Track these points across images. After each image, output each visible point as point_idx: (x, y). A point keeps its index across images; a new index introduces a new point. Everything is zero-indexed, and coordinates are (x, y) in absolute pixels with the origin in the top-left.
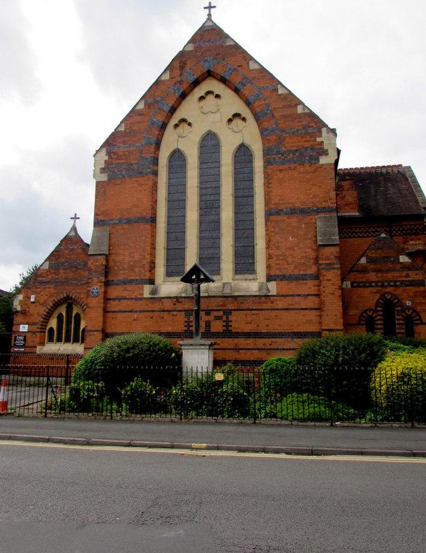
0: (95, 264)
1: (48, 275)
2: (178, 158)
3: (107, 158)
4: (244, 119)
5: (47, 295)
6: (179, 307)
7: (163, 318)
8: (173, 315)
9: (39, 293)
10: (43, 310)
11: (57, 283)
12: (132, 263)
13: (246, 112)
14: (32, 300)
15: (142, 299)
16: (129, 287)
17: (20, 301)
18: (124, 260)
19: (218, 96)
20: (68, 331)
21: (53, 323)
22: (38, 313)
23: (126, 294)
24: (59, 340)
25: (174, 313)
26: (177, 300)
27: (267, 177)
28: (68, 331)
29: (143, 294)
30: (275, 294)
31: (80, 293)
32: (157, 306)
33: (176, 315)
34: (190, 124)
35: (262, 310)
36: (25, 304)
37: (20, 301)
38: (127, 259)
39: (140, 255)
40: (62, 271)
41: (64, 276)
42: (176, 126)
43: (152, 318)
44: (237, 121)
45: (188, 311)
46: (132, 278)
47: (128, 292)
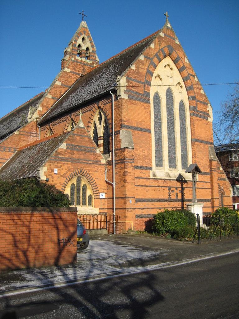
0: (129, 154)
1: (65, 154)
2: (157, 96)
5: (66, 169)
6: (166, 185)
7: (159, 190)
8: (163, 189)
9: (60, 167)
10: (63, 180)
12: (144, 156)
13: (182, 83)
14: (56, 172)
15: (150, 179)
16: (144, 171)
17: (45, 172)
18: (140, 153)
19: (171, 69)
20: (78, 197)
22: (60, 183)
23: (142, 175)
25: (164, 188)
26: (165, 181)
28: (78, 197)
29: (150, 176)
30: (198, 181)
31: (89, 170)
32: (156, 184)
33: (165, 189)
34: (161, 79)
35: (154, 186)
36: (49, 175)
37: (45, 172)
38: (142, 154)
39: (147, 152)
40: (75, 152)
41: (77, 156)
42: (156, 77)
43: (154, 190)
45: (169, 187)
46: (145, 166)
47: (143, 174)
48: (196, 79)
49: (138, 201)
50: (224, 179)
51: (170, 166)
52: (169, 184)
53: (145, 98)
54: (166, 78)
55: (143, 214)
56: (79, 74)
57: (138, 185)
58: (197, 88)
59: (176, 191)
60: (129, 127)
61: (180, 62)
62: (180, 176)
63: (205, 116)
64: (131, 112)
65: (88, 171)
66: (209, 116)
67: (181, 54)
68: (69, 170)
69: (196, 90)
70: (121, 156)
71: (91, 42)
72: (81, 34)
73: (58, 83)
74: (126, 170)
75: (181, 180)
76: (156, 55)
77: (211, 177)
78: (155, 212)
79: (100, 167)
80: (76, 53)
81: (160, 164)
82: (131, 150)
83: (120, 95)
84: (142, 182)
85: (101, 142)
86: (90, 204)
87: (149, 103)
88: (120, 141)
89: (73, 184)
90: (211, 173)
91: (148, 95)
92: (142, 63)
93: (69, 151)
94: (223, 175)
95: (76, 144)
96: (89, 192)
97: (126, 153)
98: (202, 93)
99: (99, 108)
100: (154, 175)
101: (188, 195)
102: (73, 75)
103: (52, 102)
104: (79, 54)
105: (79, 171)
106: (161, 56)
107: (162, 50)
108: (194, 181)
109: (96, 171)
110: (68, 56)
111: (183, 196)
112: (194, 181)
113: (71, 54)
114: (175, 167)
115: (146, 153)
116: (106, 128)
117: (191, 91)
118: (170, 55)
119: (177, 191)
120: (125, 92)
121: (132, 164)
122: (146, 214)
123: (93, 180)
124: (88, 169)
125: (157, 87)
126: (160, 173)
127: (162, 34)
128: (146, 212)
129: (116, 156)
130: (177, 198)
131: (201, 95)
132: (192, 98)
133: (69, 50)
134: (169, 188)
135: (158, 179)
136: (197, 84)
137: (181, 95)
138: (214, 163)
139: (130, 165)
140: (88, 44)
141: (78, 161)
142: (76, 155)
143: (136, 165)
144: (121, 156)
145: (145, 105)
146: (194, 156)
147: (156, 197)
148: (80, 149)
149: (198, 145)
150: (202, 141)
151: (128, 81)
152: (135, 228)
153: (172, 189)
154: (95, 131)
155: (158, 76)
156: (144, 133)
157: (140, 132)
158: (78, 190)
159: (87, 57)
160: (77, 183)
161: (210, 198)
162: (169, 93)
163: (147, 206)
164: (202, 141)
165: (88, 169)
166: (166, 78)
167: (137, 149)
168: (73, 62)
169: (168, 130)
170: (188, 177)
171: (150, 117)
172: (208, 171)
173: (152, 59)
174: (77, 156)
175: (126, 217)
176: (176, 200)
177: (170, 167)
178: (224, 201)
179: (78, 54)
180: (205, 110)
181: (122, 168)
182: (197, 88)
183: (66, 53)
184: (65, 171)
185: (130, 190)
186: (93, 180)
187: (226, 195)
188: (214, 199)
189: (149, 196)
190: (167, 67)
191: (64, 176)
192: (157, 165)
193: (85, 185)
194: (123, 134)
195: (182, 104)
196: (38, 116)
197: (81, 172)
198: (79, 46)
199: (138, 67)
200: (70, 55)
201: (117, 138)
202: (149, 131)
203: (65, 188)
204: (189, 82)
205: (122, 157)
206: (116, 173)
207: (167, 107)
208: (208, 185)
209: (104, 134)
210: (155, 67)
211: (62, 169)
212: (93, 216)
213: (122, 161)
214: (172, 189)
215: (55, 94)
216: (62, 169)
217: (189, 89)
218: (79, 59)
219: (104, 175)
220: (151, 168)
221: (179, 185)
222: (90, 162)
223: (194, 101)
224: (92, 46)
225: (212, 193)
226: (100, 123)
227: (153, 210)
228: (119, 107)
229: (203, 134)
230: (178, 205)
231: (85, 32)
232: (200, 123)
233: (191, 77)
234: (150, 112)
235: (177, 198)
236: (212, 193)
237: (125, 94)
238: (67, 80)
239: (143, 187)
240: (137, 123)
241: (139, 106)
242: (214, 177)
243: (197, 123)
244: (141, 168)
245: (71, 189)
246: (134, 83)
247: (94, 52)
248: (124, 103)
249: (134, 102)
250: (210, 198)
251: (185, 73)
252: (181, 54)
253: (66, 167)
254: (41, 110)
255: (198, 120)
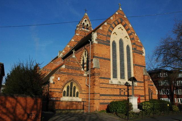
2: (114, 43)
3: (97, 36)
4: (128, 38)
10: (63, 84)
11: (68, 74)
13: (128, 37)
14: (59, 79)
16: (105, 80)
19: (122, 30)
20: (71, 92)
21: (65, 89)
23: (104, 82)
24: (68, 96)
25: (117, 89)
27: (134, 56)
28: (71, 92)
32: (112, 87)
34: (116, 35)
36: (55, 81)
41: (71, 72)
42: (113, 33)
44: (126, 38)
46: (106, 77)
48: (136, 35)
49: (101, 95)
50: (152, 85)
51: (121, 78)
52: (120, 87)
53: (107, 43)
54: (119, 34)
55: (105, 102)
56: (83, 36)
57: (102, 87)
58: (136, 39)
59: (124, 91)
60: (97, 57)
61: (127, 26)
62: (127, 83)
63: (141, 53)
64: (99, 50)
65: (76, 80)
66: (143, 53)
67: (127, 23)
68: (66, 79)
69: (136, 40)
70: (93, 72)
71: (89, 22)
72: (85, 19)
73: (73, 40)
74: (95, 79)
75: (127, 84)
76: (114, 23)
77: (145, 84)
78: (110, 101)
79: (83, 78)
80: (82, 27)
81: (115, 76)
82: (98, 69)
83: (93, 42)
84: (104, 85)
85: (85, 65)
86: (77, 96)
87: (110, 46)
88: (93, 64)
89: (68, 86)
90: (144, 82)
91: (109, 42)
92: (105, 26)
93: (66, 69)
94: (152, 83)
95: (71, 66)
96: (77, 90)
97: (95, 70)
98: (139, 41)
99: (85, 49)
100: (112, 82)
101: (130, 93)
102: (80, 36)
103: (69, 49)
104: (84, 27)
105: (72, 79)
106: (116, 23)
107: (117, 20)
108: (133, 85)
109: (81, 80)
110: (78, 28)
111: (128, 93)
112: (133, 85)
113: (79, 27)
114: (124, 78)
115: (107, 71)
116: (88, 59)
117: (133, 40)
118: (121, 23)
119: (125, 91)
120: (96, 40)
121: (99, 76)
122: (106, 102)
123: (79, 84)
124: (76, 78)
125: (114, 38)
126: (115, 81)
127: (117, 13)
128: (106, 101)
129: (91, 72)
130: (124, 94)
131: (139, 42)
132: (133, 44)
133: (79, 25)
134: (120, 89)
135: (113, 84)
136: (136, 37)
137: (127, 42)
138: (146, 77)
139: (97, 76)
140: (88, 23)
141: (72, 74)
142: (70, 71)
143: (101, 77)
144: (93, 72)
145: (107, 47)
146: (135, 73)
147: (112, 94)
148: (72, 68)
149: (136, 67)
150: (139, 66)
151: (97, 35)
152: (99, 109)
153: (122, 90)
154: (83, 60)
155: (115, 33)
156: (106, 60)
157: (104, 60)
158: (71, 89)
159: (87, 29)
160: (70, 86)
161: (144, 95)
162: (121, 42)
163: (107, 98)
164: (139, 66)
165: (76, 78)
166: (119, 34)
167: (102, 69)
168: (80, 31)
169: (120, 60)
170: (130, 83)
171: (110, 52)
172: (143, 81)
173: (111, 25)
174: (71, 72)
175: (94, 104)
176: (124, 95)
177: (121, 78)
178: (152, 97)
179: (83, 27)
180: (141, 50)
181: (93, 78)
182: (136, 39)
183: (77, 27)
184: (64, 79)
185: (97, 89)
186: (79, 84)
187: (154, 94)
188: (146, 96)
189: (108, 93)
190: (120, 29)
191: (63, 81)
192: (114, 77)
193: (74, 86)
194: (94, 60)
195: (128, 47)
196: (62, 55)
197: (72, 80)
198: (84, 24)
199: (103, 28)
200: (79, 28)
201: (91, 63)
202: (109, 60)
203: (64, 87)
204: (132, 36)
205: (93, 73)
206: (91, 81)
207: (120, 48)
208: (143, 88)
209: (87, 61)
210: (113, 28)
211: (63, 78)
212: (78, 103)
213: (93, 75)
214: (122, 90)
215: (71, 45)
216: (63, 78)
217: (132, 39)
218: (83, 29)
219: (85, 82)
220: (110, 79)
221: (126, 87)
222: (78, 75)
223: (135, 45)
224: (90, 24)
225: (145, 92)
226: (85, 56)
227: (109, 100)
228: (92, 47)
229: (139, 62)
230: (125, 98)
231: (86, 18)
232: (138, 56)
233: (133, 34)
234: (110, 50)
235: (124, 94)
236: (145, 92)
237: (96, 41)
238: (77, 39)
239: (105, 88)
240: (102, 55)
241: (104, 47)
242: (146, 84)
243: (136, 56)
244: (104, 78)
245: (67, 89)
246: (101, 36)
247: (90, 26)
248: (95, 45)
249: (101, 45)
250: (144, 95)
251: (130, 32)
252: (127, 23)
253: (64, 77)
254: (64, 52)
255: (137, 55)
